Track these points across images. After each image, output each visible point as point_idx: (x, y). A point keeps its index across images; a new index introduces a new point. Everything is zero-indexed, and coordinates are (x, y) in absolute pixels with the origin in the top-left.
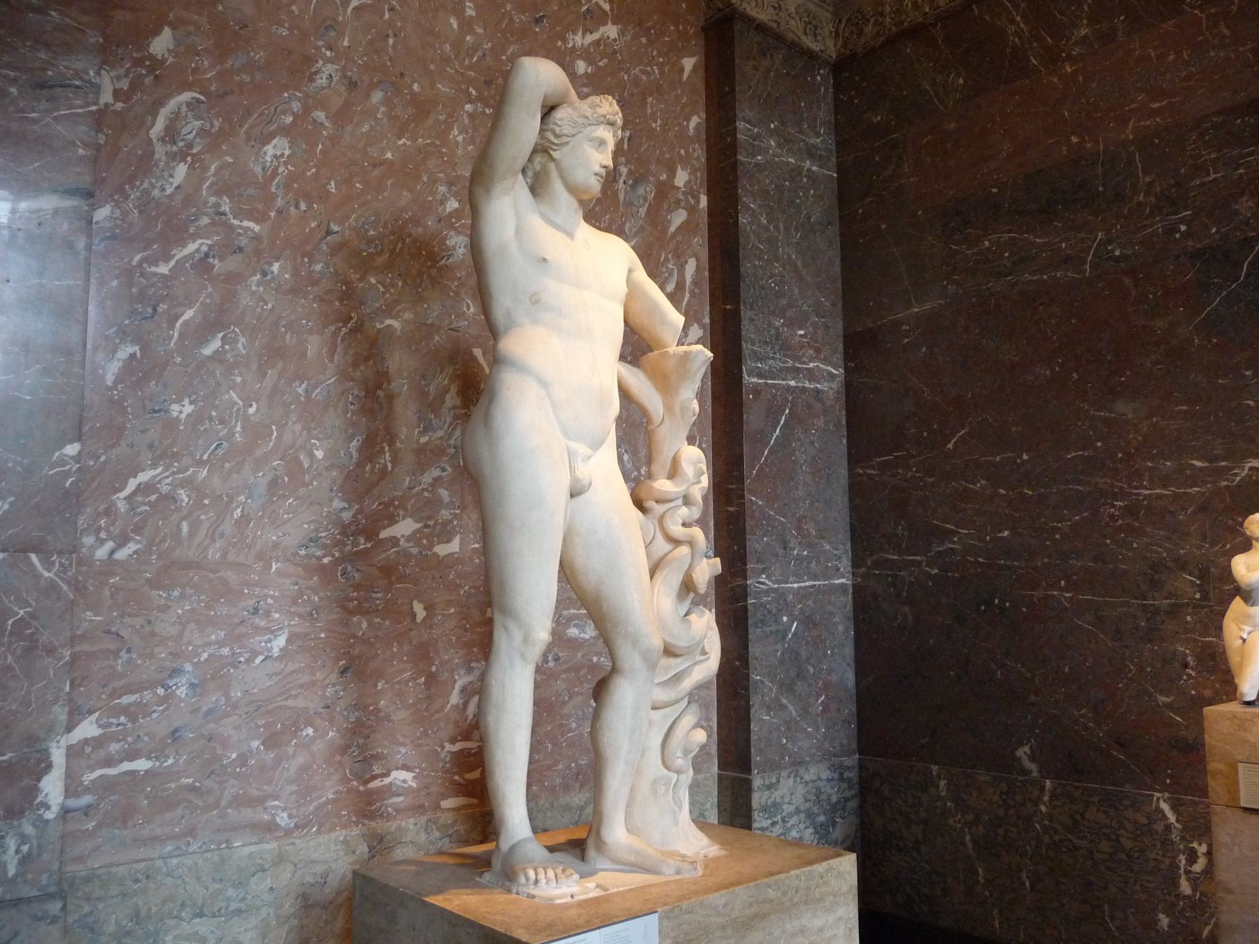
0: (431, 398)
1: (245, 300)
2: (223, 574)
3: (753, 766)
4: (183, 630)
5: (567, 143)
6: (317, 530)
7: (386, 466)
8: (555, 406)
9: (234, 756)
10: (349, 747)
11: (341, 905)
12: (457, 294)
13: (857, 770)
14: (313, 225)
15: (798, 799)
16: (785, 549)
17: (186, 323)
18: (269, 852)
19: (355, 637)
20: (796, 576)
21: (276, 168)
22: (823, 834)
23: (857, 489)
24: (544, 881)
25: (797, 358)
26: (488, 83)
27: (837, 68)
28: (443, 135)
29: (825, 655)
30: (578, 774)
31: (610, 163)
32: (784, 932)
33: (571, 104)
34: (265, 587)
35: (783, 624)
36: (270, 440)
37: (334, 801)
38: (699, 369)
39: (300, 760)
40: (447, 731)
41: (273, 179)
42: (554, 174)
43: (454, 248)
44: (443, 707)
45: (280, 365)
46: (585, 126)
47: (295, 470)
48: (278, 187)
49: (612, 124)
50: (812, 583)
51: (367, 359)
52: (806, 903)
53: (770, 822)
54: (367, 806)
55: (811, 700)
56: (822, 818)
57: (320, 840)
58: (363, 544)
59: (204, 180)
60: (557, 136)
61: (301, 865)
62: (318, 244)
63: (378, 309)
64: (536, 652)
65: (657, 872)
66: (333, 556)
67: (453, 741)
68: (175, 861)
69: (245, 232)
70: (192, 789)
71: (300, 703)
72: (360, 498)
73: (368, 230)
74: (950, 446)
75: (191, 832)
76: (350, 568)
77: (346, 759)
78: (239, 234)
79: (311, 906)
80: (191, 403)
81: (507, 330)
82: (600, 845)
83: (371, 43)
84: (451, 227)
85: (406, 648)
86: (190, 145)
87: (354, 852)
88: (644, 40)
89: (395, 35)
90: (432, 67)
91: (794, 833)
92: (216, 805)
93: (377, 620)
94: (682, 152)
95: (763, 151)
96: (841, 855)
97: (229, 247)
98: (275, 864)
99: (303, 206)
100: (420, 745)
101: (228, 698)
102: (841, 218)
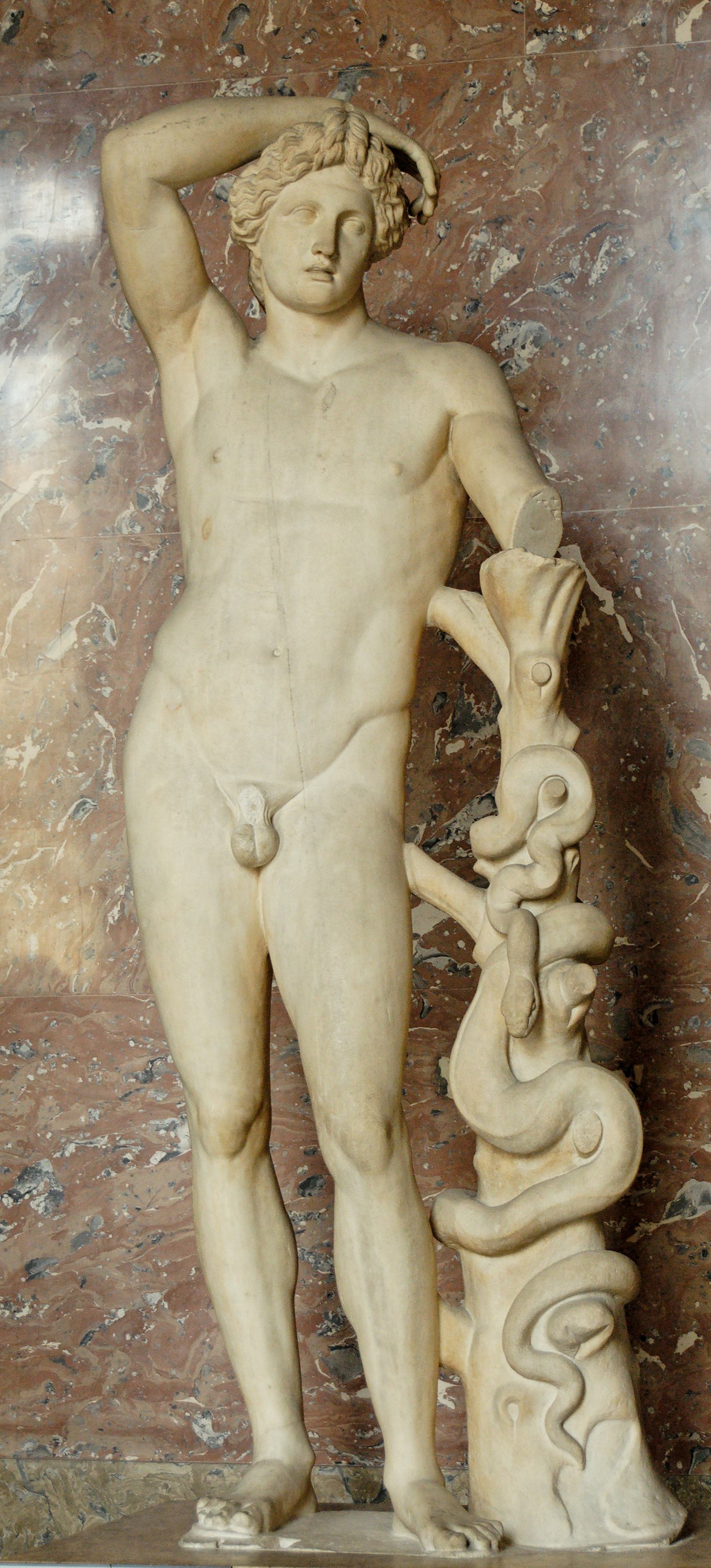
9: (121, 1313)
17: (23, 616)
18: (178, 1478)
68: (33, 1466)
70: (59, 1359)
80: (35, 742)
92: (96, 1389)
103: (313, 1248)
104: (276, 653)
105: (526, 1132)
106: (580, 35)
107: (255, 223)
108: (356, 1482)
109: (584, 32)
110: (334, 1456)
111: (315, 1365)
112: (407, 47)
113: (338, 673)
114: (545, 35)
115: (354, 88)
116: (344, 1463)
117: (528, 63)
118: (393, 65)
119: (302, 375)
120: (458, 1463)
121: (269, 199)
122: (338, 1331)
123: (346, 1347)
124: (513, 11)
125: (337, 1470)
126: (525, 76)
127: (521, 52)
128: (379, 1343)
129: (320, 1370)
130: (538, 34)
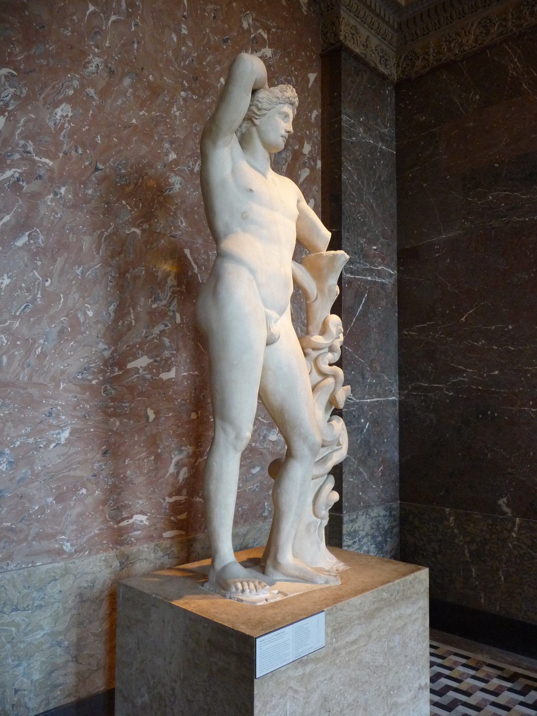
0: (159, 279)
1: (43, 210)
2: (30, 390)
3: (343, 509)
4: (4, 426)
5: (265, 114)
6: (88, 362)
7: (131, 322)
8: (259, 286)
9: (37, 508)
10: (108, 500)
11: (103, 600)
12: (175, 213)
13: (399, 509)
14: (87, 163)
15: (367, 528)
16: (363, 378)
19: (111, 430)
20: (369, 395)
21: (63, 124)
22: (380, 547)
23: (403, 344)
24: (248, 591)
25: (372, 264)
26: (196, 79)
27: (398, 86)
28: (168, 110)
29: (383, 441)
30: (242, 515)
31: (291, 129)
32: (391, 618)
33: (265, 89)
34: (56, 399)
35: (361, 423)
36: (60, 303)
37: (98, 535)
39: (78, 510)
40: (169, 489)
41: (61, 131)
43: (174, 184)
44: (164, 475)
45: (66, 255)
46: (277, 104)
47: (75, 323)
48: (64, 137)
49: (292, 104)
50: (377, 399)
51: (120, 253)
52: (403, 600)
53: (352, 541)
54: (118, 537)
55: (375, 469)
56: (380, 539)
57: (91, 559)
58: (117, 372)
59: (15, 128)
60: (259, 109)
61: (79, 576)
62: (90, 176)
63: (127, 221)
64: (243, 445)
65: (313, 582)
66: (98, 379)
67: (170, 496)
69: (43, 166)
70: (10, 529)
71: (78, 473)
73: (120, 170)
74: (463, 319)
75: (10, 557)
76: (109, 387)
77: (106, 507)
78: (39, 167)
79: (84, 601)
81: (226, 236)
82: (276, 564)
83: (123, 45)
84: (172, 170)
85: (143, 438)
86: (7, 105)
87: (111, 566)
88: (287, 60)
89: (138, 43)
90: (161, 65)
91: (365, 548)
92: (25, 539)
93: (125, 420)
94: (308, 132)
95: (357, 135)
96: (420, 569)
97: (32, 175)
98: (62, 576)
99: (80, 151)
100: (151, 499)
101: (33, 471)
102: (398, 179)
103: (108, 475)
106: (194, 97)
112: (149, 75)
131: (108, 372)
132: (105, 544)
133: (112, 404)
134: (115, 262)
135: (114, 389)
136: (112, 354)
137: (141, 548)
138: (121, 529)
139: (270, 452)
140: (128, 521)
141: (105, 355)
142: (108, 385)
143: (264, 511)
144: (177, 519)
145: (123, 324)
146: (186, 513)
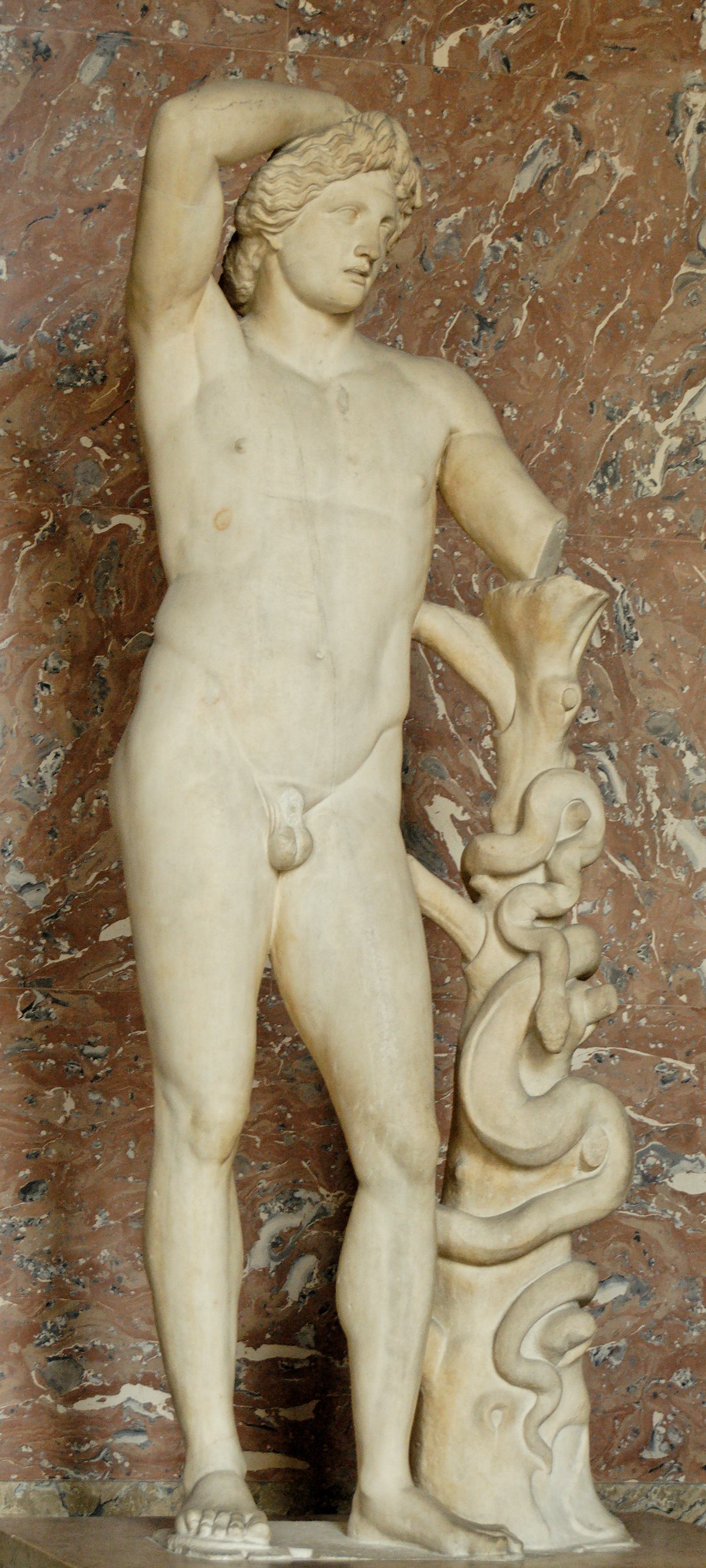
5: (290, 221)
38: (572, 617)
42: (277, 276)
51: (76, 596)
58: (66, 952)
60: (270, 212)
63: (97, 496)
72: (61, 867)
76: (40, 998)
77: (30, 1349)
93: (94, 1097)
103: (34, 1255)
104: (318, 655)
105: (548, 1145)
106: (342, 42)
107: (290, 215)
108: (72, 1497)
109: (346, 39)
110: (47, 1471)
111: (31, 1378)
112: (169, 22)
113: (371, 682)
114: (307, 36)
115: (113, 54)
116: (58, 1477)
117: (290, 61)
118: (155, 38)
119: (309, 372)
120: (175, 1475)
121: (313, 193)
122: (56, 1342)
123: (64, 1358)
124: (277, 5)
125: (53, 1485)
126: (286, 73)
127: (284, 48)
128: (391, 1352)
129: (36, 1382)
130: (301, 33)
131: (37, 953)
132: (27, 1455)
133: (51, 1046)
134: (57, 626)
135: (55, 1001)
136: (48, 899)
137: (144, 1487)
138: (80, 1419)
139: (679, 1234)
140: (103, 1400)
141: (28, 904)
142: (36, 992)
143: (649, 1443)
144: (277, 1418)
145: (87, 808)
146: (313, 1404)
